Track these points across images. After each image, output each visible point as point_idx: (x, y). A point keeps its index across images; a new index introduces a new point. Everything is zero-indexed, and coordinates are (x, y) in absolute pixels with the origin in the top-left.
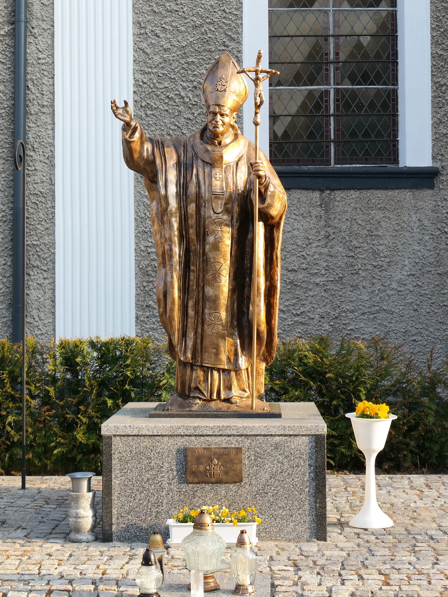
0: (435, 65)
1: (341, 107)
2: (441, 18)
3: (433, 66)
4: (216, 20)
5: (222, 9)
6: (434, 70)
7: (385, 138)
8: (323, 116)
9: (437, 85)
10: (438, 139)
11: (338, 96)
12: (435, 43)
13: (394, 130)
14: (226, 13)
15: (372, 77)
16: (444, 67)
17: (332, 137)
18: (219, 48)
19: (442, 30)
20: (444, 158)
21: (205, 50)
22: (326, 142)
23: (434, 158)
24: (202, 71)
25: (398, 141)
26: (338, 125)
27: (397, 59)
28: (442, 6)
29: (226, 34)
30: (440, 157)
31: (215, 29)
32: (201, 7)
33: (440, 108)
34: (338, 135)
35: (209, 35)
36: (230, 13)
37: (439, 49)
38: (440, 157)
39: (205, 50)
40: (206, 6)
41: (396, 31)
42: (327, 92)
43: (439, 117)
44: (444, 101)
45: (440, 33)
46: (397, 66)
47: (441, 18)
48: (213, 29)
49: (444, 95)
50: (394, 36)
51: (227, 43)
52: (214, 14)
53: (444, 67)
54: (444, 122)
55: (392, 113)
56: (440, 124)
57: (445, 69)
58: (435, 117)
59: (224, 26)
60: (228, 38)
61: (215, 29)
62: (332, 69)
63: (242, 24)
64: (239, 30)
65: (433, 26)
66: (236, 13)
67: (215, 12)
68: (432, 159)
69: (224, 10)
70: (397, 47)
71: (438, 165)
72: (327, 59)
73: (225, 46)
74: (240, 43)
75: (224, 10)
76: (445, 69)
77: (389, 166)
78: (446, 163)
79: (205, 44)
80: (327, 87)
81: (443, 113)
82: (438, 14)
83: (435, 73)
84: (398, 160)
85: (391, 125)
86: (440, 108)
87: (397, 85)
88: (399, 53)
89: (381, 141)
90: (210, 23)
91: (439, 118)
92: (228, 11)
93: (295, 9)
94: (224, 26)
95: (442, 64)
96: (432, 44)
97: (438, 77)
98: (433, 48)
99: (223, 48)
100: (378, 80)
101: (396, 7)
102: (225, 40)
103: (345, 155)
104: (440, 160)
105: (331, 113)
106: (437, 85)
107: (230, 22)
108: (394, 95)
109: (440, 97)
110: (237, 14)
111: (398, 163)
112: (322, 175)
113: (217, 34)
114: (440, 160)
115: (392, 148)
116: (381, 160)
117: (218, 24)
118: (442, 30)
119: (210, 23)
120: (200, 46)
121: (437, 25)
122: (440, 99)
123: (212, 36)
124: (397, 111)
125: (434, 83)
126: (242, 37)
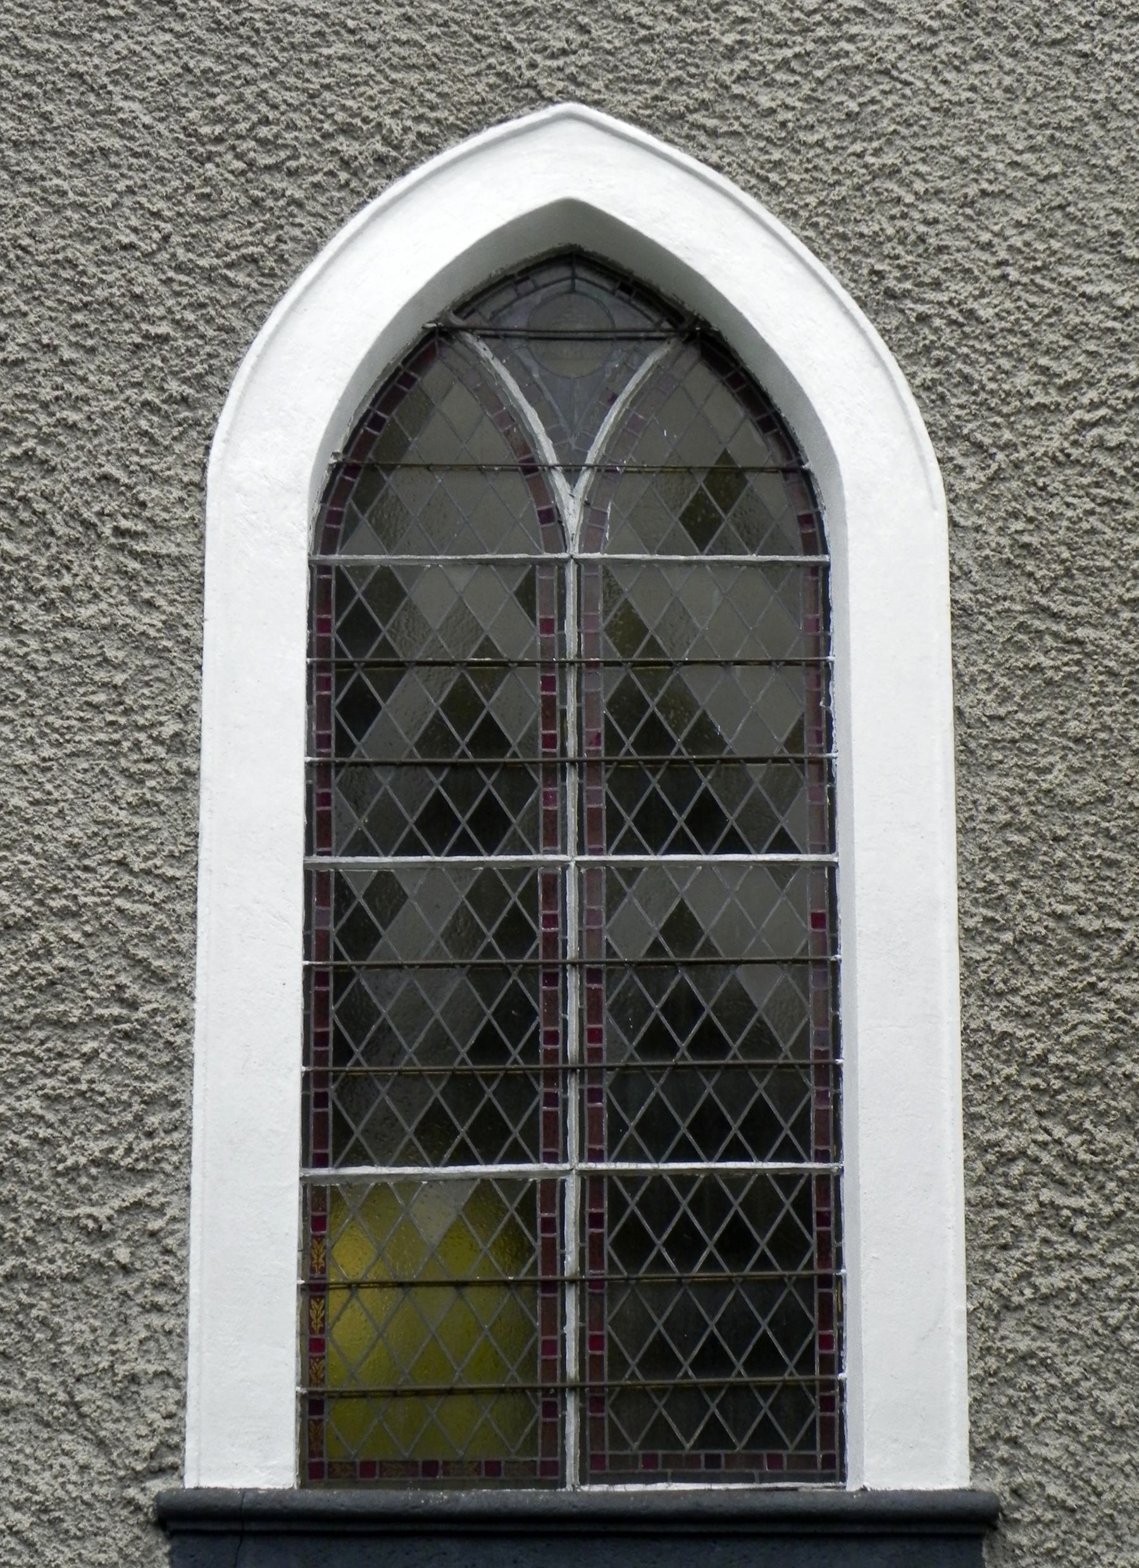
0: (979, 1077)
1: (607, 1247)
2: (1003, 889)
3: (971, 1079)
4: (90, 900)
5: (116, 855)
6: (978, 1096)
7: (791, 1374)
8: (533, 1284)
9: (990, 1157)
10: (995, 1378)
11: (596, 1201)
12: (977, 987)
13: (826, 1342)
14: (131, 872)
15: (735, 1127)
16: (1018, 1085)
17: (572, 1369)
18: (98, 1011)
19: (1008, 937)
20: (1020, 1454)
21: (40, 1021)
22: (546, 1390)
23: (978, 1454)
24: (23, 1106)
25: (842, 1385)
26: (597, 1323)
27: (837, 1053)
28: (1008, 843)
29: (127, 955)
30: (1004, 1451)
31: (87, 935)
32: (30, 850)
33: (1005, 1247)
34: (596, 1361)
35: (60, 960)
36: (148, 872)
37: (996, 1014)
38: (1004, 1451)
39: (40, 1021)
40: (51, 847)
41: (835, 947)
42: (552, 1188)
43: (997, 1285)
44: (1019, 1222)
45: (998, 948)
46: (837, 1083)
47: (1003, 889)
48: (76, 936)
49: (1021, 1196)
50: (822, 963)
51: (134, 990)
52: (84, 875)
53: (1018, 1085)
54: (1020, 1307)
55: (817, 1270)
56: (1007, 1315)
57: (1020, 1093)
58: (981, 1284)
59: (120, 924)
60: (138, 971)
61: (87, 935)
62: (573, 1096)
63: (193, 916)
64: (184, 940)
65: (970, 923)
66: (170, 872)
67: (86, 869)
68: (973, 1458)
69: (122, 863)
70: (836, 1006)
71: (995, 1484)
72: (551, 1056)
73: (122, 1002)
74: (184, 991)
75: (122, 863)
76: (1020, 1093)
77: (804, 1486)
78: (1028, 1476)
79: (41, 998)
80: (552, 1166)
81: (1016, 1270)
82: (991, 876)
83: (982, 1109)
84: (843, 1465)
85: (815, 1320)
86: (1005, 1247)
87: (838, 1158)
88: (844, 1031)
89: (771, 1388)
90: (64, 914)
91: (998, 1292)
92: (137, 865)
93: (425, 858)
94: (120, 924)
95: (1007, 1071)
96: (966, 993)
97: (995, 1125)
98: (973, 1010)
99: (116, 1010)
100: (760, 1135)
101: (832, 849)
102: (123, 979)
103: (626, 1445)
104: (1003, 1461)
105: (567, 1273)
106: (990, 1157)
107: (146, 908)
108: (824, 1197)
109: (1002, 1205)
110: (173, 879)
111: (843, 1478)
112: (511, 1528)
113: (92, 954)
114: (1003, 1461)
115: (817, 1413)
116: (775, 1462)
117: (99, 918)
118: (1008, 937)
119: (64, 914)
120: (21, 1002)
121: (988, 920)
122: (1003, 1212)
123: (71, 964)
124: (840, 1264)
125: (976, 1147)
126: (192, 969)
